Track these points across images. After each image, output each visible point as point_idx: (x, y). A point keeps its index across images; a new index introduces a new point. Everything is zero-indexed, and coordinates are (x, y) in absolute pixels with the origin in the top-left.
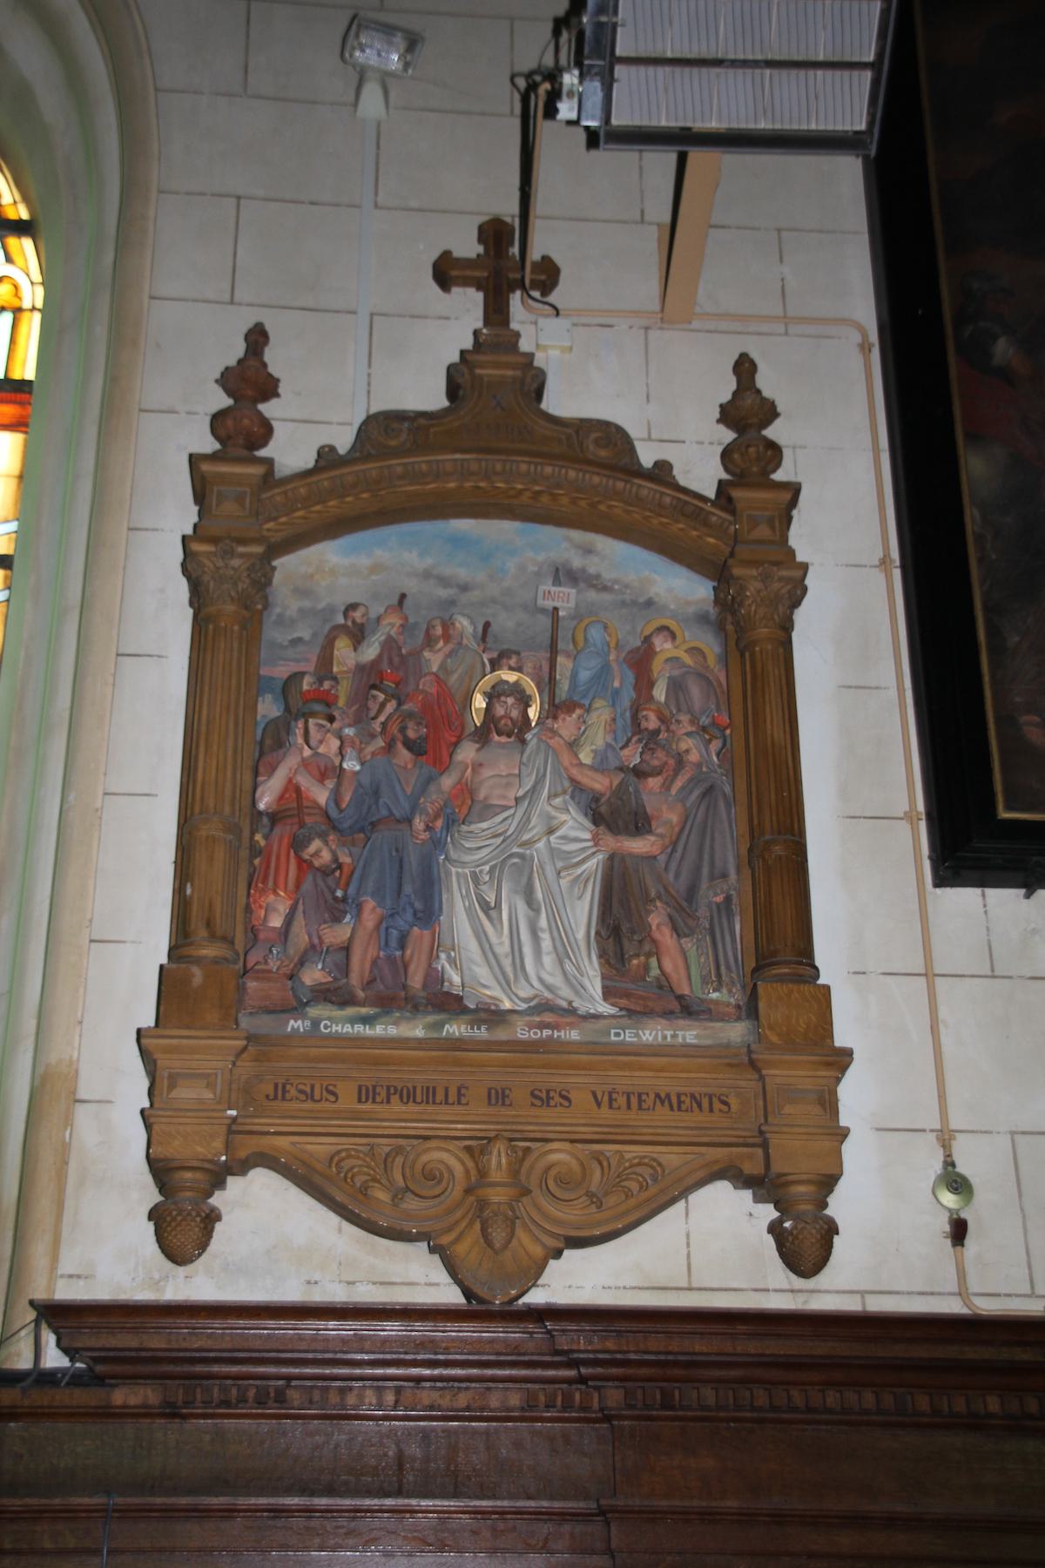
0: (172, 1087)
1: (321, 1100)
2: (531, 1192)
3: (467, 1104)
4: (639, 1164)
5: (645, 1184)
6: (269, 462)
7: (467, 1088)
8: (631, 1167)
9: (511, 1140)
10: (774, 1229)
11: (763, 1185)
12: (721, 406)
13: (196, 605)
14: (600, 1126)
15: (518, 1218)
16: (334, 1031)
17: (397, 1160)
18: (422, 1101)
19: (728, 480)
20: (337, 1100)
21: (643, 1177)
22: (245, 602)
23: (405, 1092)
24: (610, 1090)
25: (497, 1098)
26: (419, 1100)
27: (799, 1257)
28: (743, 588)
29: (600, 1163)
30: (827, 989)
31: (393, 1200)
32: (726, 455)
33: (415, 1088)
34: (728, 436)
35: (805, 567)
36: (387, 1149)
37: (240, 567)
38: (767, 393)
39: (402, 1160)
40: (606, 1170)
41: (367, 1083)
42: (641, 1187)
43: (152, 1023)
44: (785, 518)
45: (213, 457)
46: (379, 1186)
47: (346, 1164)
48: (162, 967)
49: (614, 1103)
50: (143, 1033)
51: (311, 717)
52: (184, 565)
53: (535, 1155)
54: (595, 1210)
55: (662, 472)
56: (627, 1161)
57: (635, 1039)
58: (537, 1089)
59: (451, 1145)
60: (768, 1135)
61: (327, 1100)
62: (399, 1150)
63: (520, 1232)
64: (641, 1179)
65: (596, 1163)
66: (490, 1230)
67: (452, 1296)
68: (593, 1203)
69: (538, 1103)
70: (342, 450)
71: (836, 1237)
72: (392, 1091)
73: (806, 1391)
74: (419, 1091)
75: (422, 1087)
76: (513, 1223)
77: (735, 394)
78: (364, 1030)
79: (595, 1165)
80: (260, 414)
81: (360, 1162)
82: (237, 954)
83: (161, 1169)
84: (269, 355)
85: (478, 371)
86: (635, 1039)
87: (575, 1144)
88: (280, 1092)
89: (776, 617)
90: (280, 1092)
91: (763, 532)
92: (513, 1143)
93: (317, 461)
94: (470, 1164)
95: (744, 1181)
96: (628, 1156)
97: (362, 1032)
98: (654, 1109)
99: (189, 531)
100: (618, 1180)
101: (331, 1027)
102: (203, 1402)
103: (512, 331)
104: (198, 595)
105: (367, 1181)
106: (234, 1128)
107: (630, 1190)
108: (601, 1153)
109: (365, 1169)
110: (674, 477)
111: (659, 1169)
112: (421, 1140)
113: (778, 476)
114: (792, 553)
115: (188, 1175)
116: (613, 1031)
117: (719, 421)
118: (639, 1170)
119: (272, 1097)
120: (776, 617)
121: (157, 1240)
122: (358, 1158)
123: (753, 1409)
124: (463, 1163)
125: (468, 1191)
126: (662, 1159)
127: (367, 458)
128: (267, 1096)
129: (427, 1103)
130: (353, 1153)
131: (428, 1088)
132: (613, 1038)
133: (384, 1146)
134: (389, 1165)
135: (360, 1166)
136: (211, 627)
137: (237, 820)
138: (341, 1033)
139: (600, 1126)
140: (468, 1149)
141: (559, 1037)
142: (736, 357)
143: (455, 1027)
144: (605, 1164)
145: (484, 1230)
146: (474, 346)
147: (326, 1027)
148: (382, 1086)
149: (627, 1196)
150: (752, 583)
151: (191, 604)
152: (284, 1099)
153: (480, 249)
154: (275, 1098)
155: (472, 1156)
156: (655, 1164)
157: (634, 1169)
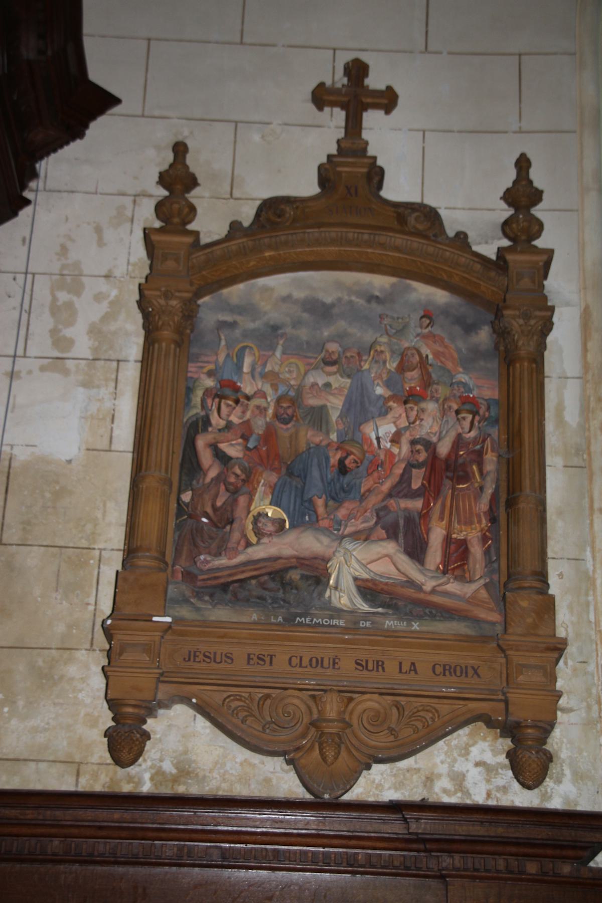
0: (120, 654)
1: (221, 662)
3: (339, 669)
4: (423, 710)
5: (426, 724)
6: (196, 234)
7: (339, 659)
9: (340, 691)
10: (510, 755)
12: (160, 173)
14: (221, 675)
15: (343, 743)
16: (334, 624)
17: (266, 703)
20: (232, 662)
21: (425, 719)
22: (179, 331)
23: (314, 660)
24: (195, 650)
25: (462, 673)
29: (398, 709)
30: (552, 598)
34: (506, 212)
36: (261, 695)
37: (176, 305)
40: (401, 713)
44: (167, 171)
45: (161, 230)
47: (234, 704)
48: (117, 572)
49: (197, 658)
52: (140, 304)
53: (356, 701)
55: (461, 238)
58: (208, 652)
60: (508, 695)
61: (225, 661)
62: (267, 696)
64: (424, 720)
66: (324, 750)
67: (308, 797)
68: (392, 734)
69: (361, 668)
70: (246, 224)
73: (495, 859)
76: (339, 746)
77: (515, 182)
78: (339, 623)
79: (395, 711)
81: (242, 704)
82: (166, 564)
83: (113, 704)
84: (190, 160)
85: (339, 169)
87: (384, 697)
92: (341, 694)
95: (490, 723)
97: (338, 624)
102: (335, 863)
103: (363, 140)
105: (246, 716)
106: (162, 679)
107: (416, 727)
111: (436, 715)
112: (282, 691)
113: (190, 227)
115: (530, 731)
116: (361, 622)
118: (421, 714)
119: (187, 659)
122: (240, 700)
123: (486, 871)
129: (444, 675)
130: (238, 697)
131: (222, 653)
132: (361, 625)
133: (259, 693)
134: (260, 706)
135: (244, 706)
137: (169, 476)
139: (221, 675)
143: (303, 619)
145: (321, 750)
146: (338, 150)
148: (296, 657)
150: (514, 321)
152: (194, 661)
153: (345, 81)
155: (315, 702)
156: (433, 711)
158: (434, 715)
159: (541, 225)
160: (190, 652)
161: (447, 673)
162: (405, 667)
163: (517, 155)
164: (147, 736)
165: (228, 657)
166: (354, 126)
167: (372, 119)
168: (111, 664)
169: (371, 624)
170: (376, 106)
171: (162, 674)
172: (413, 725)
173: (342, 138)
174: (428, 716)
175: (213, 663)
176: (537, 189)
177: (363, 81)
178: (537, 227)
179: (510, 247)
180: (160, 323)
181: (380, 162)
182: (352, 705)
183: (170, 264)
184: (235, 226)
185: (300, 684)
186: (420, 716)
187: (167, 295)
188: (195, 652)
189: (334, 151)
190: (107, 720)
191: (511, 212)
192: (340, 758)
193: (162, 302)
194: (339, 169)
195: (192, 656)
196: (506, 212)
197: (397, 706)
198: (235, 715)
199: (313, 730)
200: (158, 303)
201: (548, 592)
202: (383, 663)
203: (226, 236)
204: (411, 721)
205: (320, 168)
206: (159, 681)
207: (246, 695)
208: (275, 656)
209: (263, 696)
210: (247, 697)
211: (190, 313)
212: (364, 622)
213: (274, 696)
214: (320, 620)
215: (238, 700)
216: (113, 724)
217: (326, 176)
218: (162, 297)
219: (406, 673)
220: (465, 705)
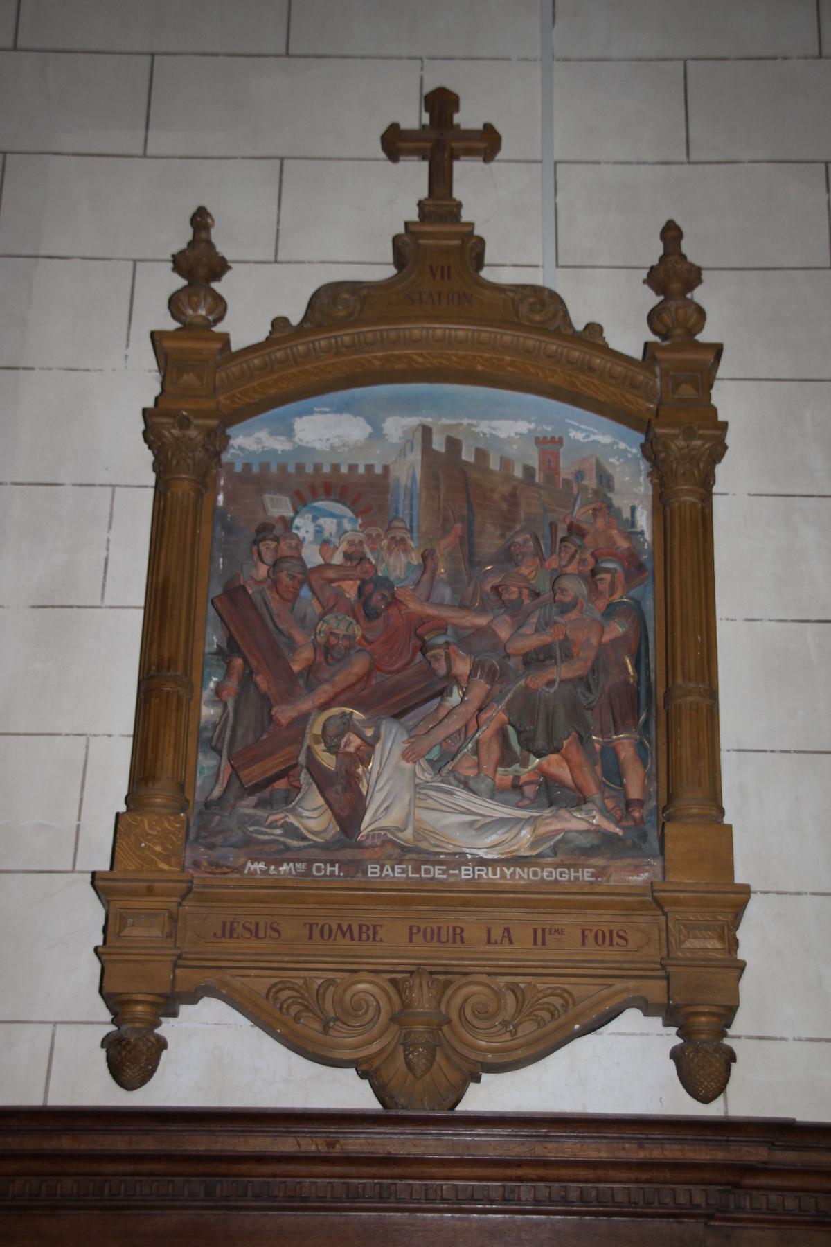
2: (449, 1022)
4: (552, 994)
6: (225, 339)
8: (545, 997)
9: (431, 973)
10: (675, 1055)
11: (672, 1015)
13: (158, 471)
18: (448, 941)
19: (654, 343)
20: (280, 936)
21: (554, 1006)
23: (600, 934)
26: (443, 939)
27: (699, 1084)
28: (667, 448)
31: (324, 1028)
32: (654, 318)
33: (439, 929)
34: (653, 299)
35: (724, 426)
36: (320, 982)
38: (692, 258)
39: (334, 989)
41: (368, 924)
42: (553, 1015)
43: (106, 867)
44: (182, 252)
46: (312, 1015)
48: (118, 815)
50: (97, 876)
51: (307, 567)
52: (145, 434)
54: (510, 1038)
55: (594, 329)
56: (541, 991)
57: (444, 876)
59: (382, 979)
60: (669, 969)
62: (330, 982)
63: (439, 1057)
65: (511, 994)
70: (295, 320)
71: (733, 1064)
72: (415, 930)
74: (444, 932)
75: (448, 927)
77: (662, 259)
80: (213, 291)
84: (686, 247)
85: (422, 242)
86: (418, 876)
88: (227, 932)
89: (696, 472)
90: (227, 932)
91: (687, 391)
92: (434, 976)
93: (271, 333)
94: (394, 995)
95: (648, 1009)
96: (540, 987)
98: (501, 943)
99: (150, 403)
100: (531, 1010)
101: (569, 874)
103: (455, 200)
104: (161, 467)
105: (299, 1012)
108: (516, 984)
109: (300, 1001)
110: (604, 338)
114: (714, 410)
115: (703, 1019)
117: (644, 282)
119: (219, 933)
120: (696, 472)
121: (108, 1066)
122: (292, 989)
124: (390, 998)
125: (394, 1019)
126: (576, 991)
127: (319, 328)
128: (215, 934)
130: (288, 985)
136: (169, 494)
138: (515, 867)
140: (393, 982)
141: (577, 878)
142: (663, 223)
144: (519, 994)
146: (419, 216)
147: (319, 869)
149: (539, 1025)
151: (154, 470)
152: (231, 936)
154: (223, 935)
156: (566, 995)
157: (545, 1000)
158: (567, 1002)
159: (701, 313)
160: (224, 923)
161: (458, 937)
162: (497, 933)
163: (193, 209)
164: (162, 1044)
165: (250, 931)
166: (440, 180)
167: (468, 176)
168: (108, 944)
169: (593, 875)
170: (470, 152)
171: (180, 957)
172: (535, 1015)
173: (426, 199)
174: (558, 1001)
175: (253, 938)
176: (692, 265)
177: (452, 118)
178: (694, 318)
179: (178, 329)
180: (174, 462)
181: (477, 232)
182: (449, 992)
183: (189, 378)
184: (279, 323)
185: (288, 962)
186: (548, 1003)
187: (184, 423)
188: (232, 924)
189: (413, 215)
190: (102, 1022)
191: (662, 298)
192: (435, 1066)
193: (176, 432)
194: (422, 242)
195: (228, 931)
196: (653, 299)
197: (513, 988)
198: (284, 1011)
199: (394, 1028)
200: (172, 435)
201: (722, 821)
202: (462, 930)
203: (267, 339)
204: (536, 1010)
205: (396, 240)
206: (176, 966)
207: (301, 982)
208: (382, 926)
209: (321, 984)
210: (301, 984)
211: (216, 441)
212: (539, 870)
213: (339, 981)
214: (291, 864)
215: (289, 988)
216: (680, 1041)
217: (403, 249)
218: (176, 425)
219: (496, 943)
220: (610, 986)
